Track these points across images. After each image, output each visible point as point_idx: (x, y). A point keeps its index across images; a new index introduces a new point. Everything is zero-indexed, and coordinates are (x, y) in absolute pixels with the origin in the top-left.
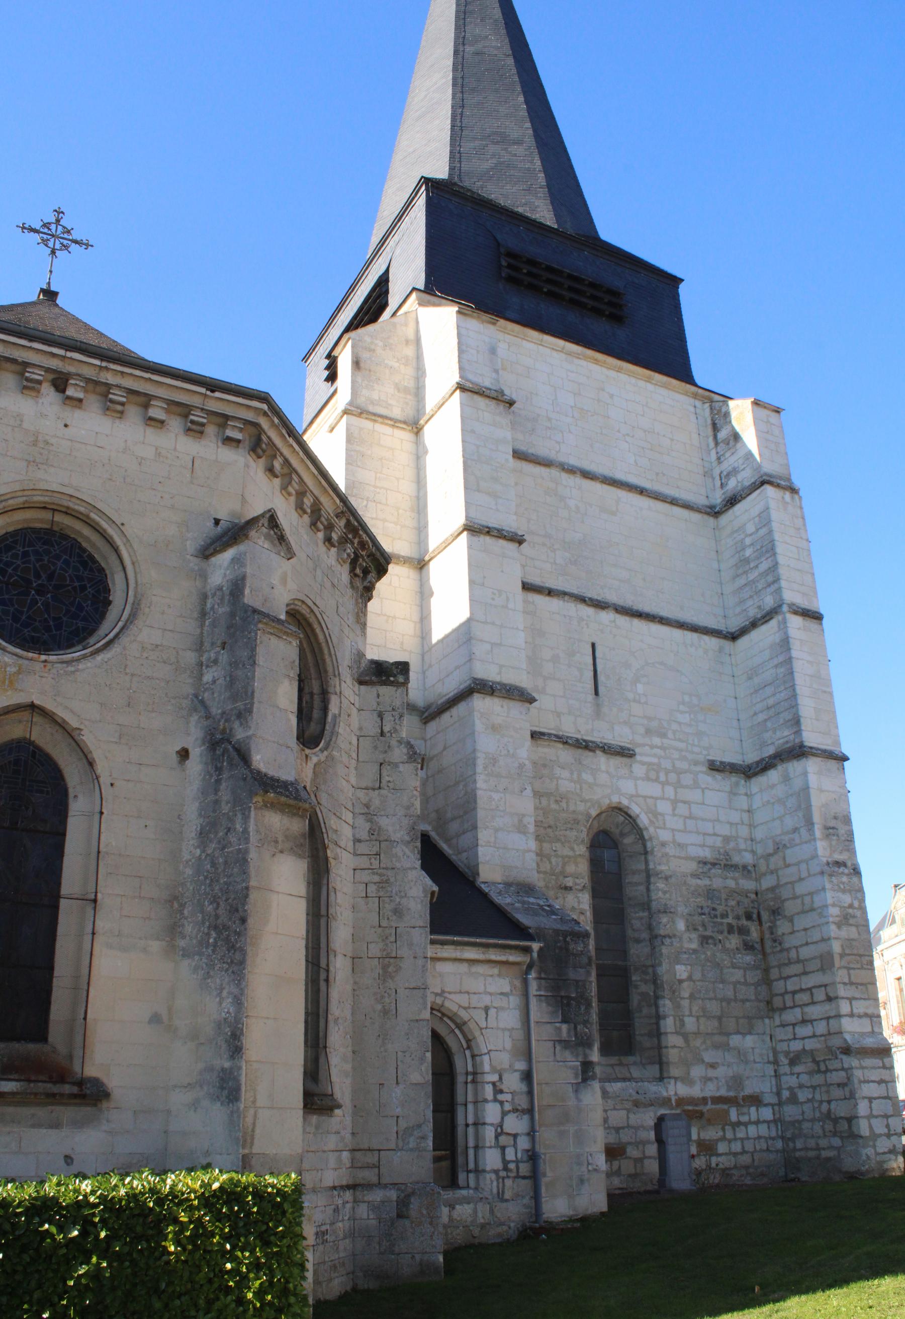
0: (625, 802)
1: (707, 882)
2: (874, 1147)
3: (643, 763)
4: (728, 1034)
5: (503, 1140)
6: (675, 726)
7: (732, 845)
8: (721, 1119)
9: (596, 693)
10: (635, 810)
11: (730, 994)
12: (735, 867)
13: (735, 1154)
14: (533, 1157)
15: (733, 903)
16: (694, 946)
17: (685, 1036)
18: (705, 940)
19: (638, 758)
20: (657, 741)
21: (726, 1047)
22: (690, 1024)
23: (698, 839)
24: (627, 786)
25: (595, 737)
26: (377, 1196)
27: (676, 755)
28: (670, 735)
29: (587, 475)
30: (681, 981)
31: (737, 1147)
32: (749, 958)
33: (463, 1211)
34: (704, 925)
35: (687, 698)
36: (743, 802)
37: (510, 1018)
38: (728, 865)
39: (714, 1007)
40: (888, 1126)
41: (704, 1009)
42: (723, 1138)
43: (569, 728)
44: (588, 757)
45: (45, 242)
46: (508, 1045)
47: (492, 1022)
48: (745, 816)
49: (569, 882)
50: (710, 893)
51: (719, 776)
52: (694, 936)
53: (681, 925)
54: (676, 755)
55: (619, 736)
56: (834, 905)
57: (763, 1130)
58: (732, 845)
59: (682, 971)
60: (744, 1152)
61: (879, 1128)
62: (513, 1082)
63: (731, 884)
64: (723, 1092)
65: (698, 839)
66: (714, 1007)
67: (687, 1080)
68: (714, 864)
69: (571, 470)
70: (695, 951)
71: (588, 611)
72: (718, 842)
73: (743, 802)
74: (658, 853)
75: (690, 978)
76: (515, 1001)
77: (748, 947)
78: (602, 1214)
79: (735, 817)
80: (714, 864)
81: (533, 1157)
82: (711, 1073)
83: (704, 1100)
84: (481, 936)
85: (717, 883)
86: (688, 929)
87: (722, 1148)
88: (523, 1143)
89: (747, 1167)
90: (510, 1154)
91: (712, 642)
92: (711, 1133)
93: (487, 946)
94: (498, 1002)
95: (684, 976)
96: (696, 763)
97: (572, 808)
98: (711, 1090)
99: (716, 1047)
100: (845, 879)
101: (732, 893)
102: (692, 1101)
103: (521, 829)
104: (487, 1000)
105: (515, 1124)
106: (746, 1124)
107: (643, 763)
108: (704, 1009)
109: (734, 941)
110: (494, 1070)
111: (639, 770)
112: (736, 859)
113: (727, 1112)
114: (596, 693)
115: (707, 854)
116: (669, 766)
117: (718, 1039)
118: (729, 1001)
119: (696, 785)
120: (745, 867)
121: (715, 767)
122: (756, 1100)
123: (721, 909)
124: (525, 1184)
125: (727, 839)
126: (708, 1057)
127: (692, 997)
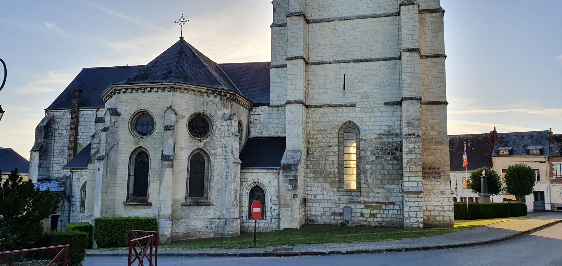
0: (352, 120)
1: (381, 140)
2: (410, 220)
3: (359, 107)
4: (384, 184)
5: (272, 210)
6: (373, 94)
7: (392, 128)
9: (344, 89)
10: (355, 121)
11: (386, 173)
12: (393, 134)
13: (383, 218)
15: (389, 146)
16: (373, 159)
17: (368, 185)
18: (377, 157)
19: (357, 106)
20: (365, 100)
21: (383, 188)
22: (370, 181)
23: (379, 127)
25: (343, 103)
26: (222, 220)
27: (372, 103)
28: (371, 97)
29: (346, 19)
30: (367, 169)
31: (384, 216)
32: (395, 162)
34: (378, 153)
35: (379, 84)
36: (399, 114)
37: (275, 184)
39: (380, 177)
40: (416, 215)
41: (376, 177)
42: (380, 213)
44: (340, 109)
45: (184, 24)
46: (274, 190)
47: (270, 185)
48: (399, 118)
49: (331, 144)
50: (381, 143)
51: (389, 107)
52: (374, 156)
53: (369, 153)
54: (372, 103)
55: (352, 101)
56: (406, 148)
58: (392, 128)
59: (368, 167)
60: (387, 217)
61: (412, 214)
62: (275, 198)
63: (391, 140)
64: (381, 201)
65: (379, 127)
66: (380, 177)
67: (368, 197)
68: (383, 135)
69: (340, 19)
70: (374, 161)
72: (386, 128)
73: (399, 114)
74: (362, 133)
75: (371, 168)
76: (276, 180)
78: (297, 229)
79: (395, 119)
80: (383, 135)
82: (376, 195)
83: (373, 203)
84: (134, 185)
85: (385, 140)
86: (371, 154)
87: (378, 216)
88: (277, 211)
89: (388, 222)
90: (273, 213)
91: (393, 62)
93: (268, 169)
94: (272, 180)
95: (369, 168)
96: (380, 104)
97: (333, 124)
98: (376, 200)
99: (379, 188)
100: (412, 139)
101: (390, 143)
102: (368, 202)
103: (298, 137)
104: (269, 180)
106: (388, 210)
107: (359, 107)
108: (376, 177)
110: (270, 195)
112: (393, 132)
113: (382, 206)
114: (344, 89)
115: (382, 132)
116: (369, 106)
117: (380, 185)
118: (385, 175)
119: (379, 111)
120: (396, 134)
121: (386, 104)
122: (393, 203)
123: (385, 148)
124: (276, 220)
125: (390, 126)
126: (376, 190)
127: (371, 174)
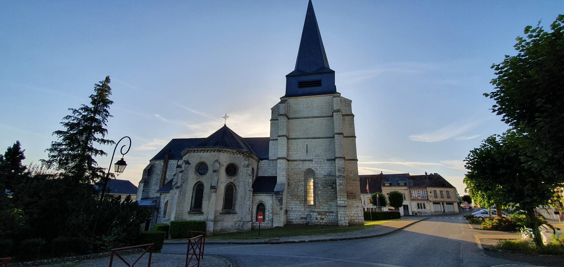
8: (326, 215)
14: (272, 219)
22: (320, 200)
24: (311, 165)
33: (263, 225)
37: (271, 202)
38: (330, 175)
39: (325, 198)
43: (302, 158)
44: (305, 162)
55: (311, 158)
57: (334, 217)
59: (319, 192)
61: (342, 219)
62: (270, 210)
71: (306, 140)
73: (334, 165)
77: (333, 188)
81: (272, 219)
85: (327, 178)
92: (323, 217)
98: (324, 210)
103: (283, 176)
105: (270, 215)
109: (330, 187)
111: (314, 163)
121: (328, 160)
122: (332, 212)
126: (324, 205)
